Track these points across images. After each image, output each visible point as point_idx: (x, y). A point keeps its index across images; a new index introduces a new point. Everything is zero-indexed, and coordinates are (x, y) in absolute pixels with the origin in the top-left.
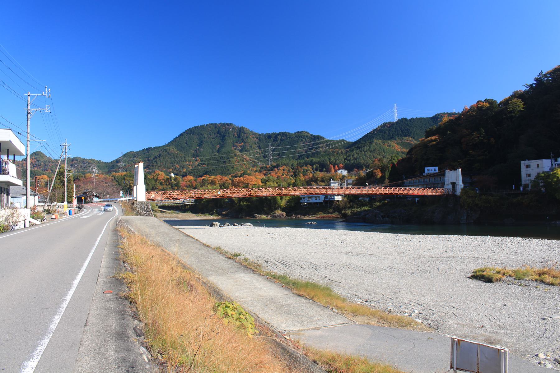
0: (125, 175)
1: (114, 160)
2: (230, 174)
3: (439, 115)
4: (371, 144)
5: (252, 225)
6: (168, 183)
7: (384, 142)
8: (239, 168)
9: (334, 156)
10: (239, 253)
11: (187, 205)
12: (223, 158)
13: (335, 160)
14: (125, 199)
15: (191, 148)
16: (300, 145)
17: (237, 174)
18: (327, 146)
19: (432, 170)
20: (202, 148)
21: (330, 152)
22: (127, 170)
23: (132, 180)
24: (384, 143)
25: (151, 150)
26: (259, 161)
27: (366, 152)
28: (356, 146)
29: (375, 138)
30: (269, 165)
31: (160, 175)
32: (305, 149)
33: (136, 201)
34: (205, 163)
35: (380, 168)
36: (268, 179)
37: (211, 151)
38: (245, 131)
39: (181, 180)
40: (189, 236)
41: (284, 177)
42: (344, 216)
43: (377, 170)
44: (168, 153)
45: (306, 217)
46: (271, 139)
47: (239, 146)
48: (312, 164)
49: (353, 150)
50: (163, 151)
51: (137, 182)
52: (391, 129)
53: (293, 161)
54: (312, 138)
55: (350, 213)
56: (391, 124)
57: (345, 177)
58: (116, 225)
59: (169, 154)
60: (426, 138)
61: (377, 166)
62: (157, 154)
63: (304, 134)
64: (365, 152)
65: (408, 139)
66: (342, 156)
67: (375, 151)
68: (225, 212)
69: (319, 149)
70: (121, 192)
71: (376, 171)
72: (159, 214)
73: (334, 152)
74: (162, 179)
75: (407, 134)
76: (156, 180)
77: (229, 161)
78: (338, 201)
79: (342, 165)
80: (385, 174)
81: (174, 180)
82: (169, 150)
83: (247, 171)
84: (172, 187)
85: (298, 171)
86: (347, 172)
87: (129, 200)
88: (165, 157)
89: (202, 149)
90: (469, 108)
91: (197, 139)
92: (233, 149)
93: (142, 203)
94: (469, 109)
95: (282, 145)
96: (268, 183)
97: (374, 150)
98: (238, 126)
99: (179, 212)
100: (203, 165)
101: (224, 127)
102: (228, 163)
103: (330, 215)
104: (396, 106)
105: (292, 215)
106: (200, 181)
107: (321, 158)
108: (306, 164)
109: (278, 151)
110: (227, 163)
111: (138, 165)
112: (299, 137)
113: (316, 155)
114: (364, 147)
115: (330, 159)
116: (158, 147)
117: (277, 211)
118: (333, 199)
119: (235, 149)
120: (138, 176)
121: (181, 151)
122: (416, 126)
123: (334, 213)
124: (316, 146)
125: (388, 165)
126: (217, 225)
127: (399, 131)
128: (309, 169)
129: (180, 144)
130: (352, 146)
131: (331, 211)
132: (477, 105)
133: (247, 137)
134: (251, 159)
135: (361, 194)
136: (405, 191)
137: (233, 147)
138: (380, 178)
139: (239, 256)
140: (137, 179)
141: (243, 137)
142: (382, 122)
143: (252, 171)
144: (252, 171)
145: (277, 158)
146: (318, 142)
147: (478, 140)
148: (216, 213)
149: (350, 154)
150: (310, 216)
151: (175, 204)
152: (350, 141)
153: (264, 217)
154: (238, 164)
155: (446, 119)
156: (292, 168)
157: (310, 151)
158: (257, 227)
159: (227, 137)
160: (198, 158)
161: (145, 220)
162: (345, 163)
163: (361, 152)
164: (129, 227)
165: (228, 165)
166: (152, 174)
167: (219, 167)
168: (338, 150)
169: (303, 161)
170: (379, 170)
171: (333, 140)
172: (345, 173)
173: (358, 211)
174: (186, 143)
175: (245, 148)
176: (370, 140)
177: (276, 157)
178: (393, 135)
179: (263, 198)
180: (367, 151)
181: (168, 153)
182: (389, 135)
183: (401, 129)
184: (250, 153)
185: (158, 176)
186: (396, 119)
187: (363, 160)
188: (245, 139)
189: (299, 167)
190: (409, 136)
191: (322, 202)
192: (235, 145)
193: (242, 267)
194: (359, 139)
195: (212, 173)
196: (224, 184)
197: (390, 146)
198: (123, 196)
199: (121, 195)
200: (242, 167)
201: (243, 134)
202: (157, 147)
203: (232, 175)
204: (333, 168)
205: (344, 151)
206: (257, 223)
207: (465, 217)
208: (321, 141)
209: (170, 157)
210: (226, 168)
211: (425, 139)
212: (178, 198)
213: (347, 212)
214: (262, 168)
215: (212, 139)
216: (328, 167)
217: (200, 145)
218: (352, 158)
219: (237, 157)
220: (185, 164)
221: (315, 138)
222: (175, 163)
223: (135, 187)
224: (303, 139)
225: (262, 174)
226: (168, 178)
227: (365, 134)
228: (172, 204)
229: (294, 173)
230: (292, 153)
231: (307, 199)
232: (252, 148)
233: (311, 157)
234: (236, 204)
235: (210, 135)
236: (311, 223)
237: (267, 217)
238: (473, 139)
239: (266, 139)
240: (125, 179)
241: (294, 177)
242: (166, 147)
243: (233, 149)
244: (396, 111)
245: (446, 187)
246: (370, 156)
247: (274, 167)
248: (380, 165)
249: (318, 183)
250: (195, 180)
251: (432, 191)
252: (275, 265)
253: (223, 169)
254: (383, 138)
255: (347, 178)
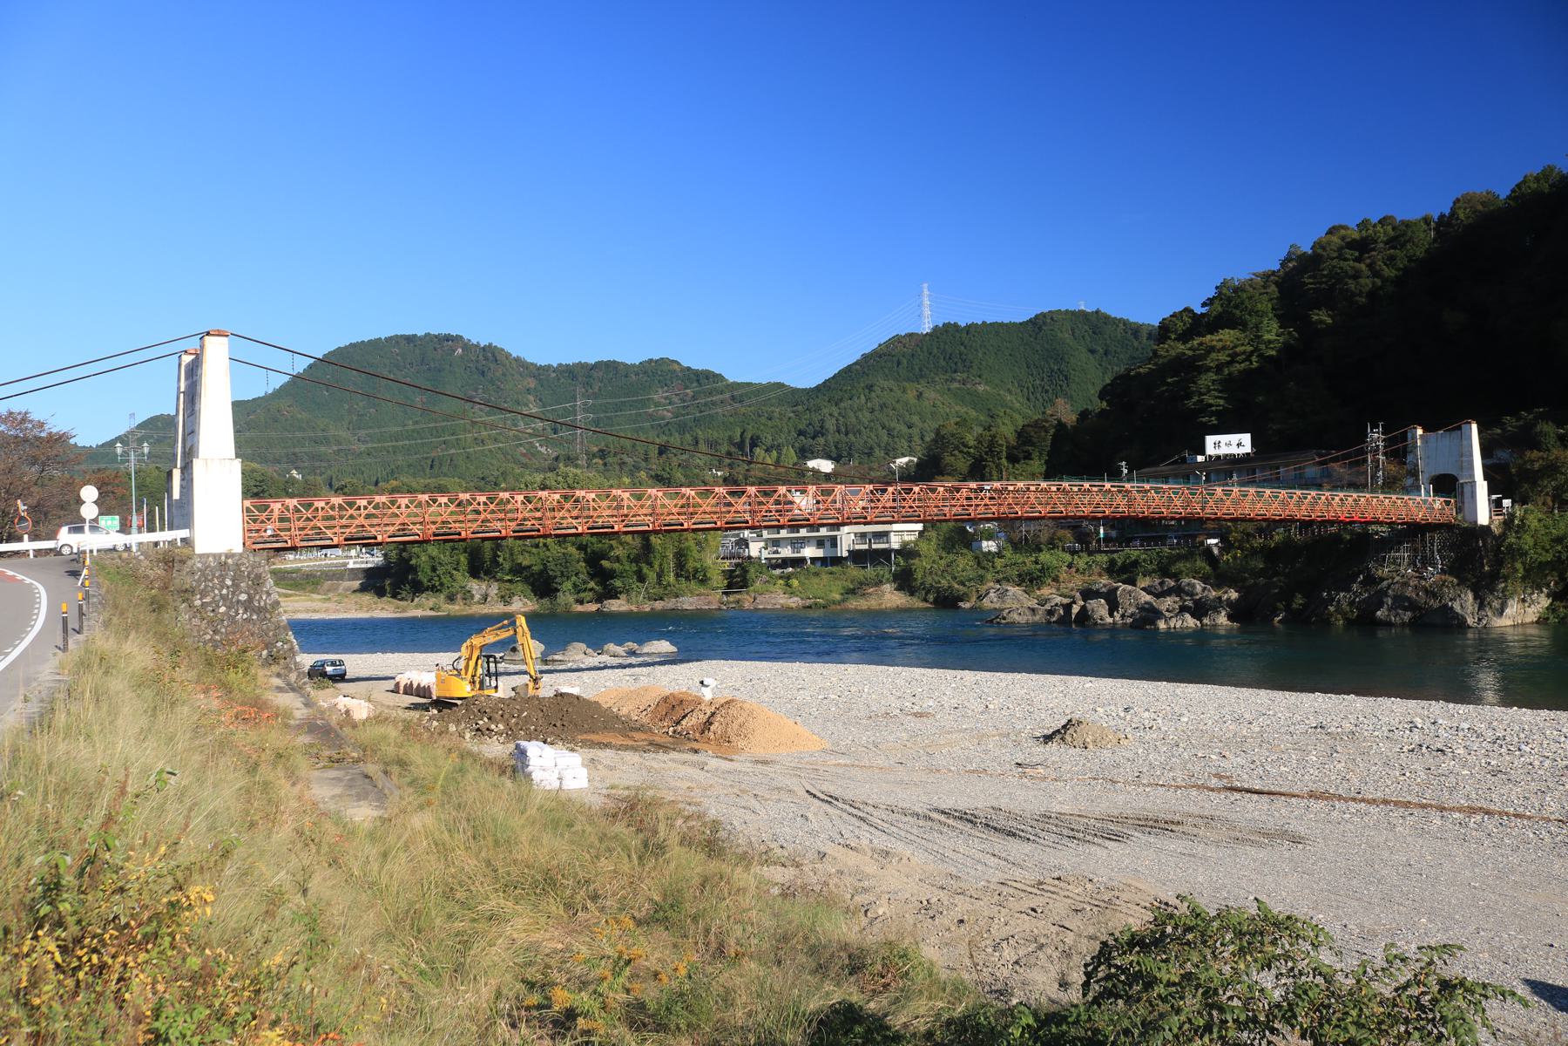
3: (1043, 315)
93: (222, 564)
171: (749, 384)
178: (921, 370)
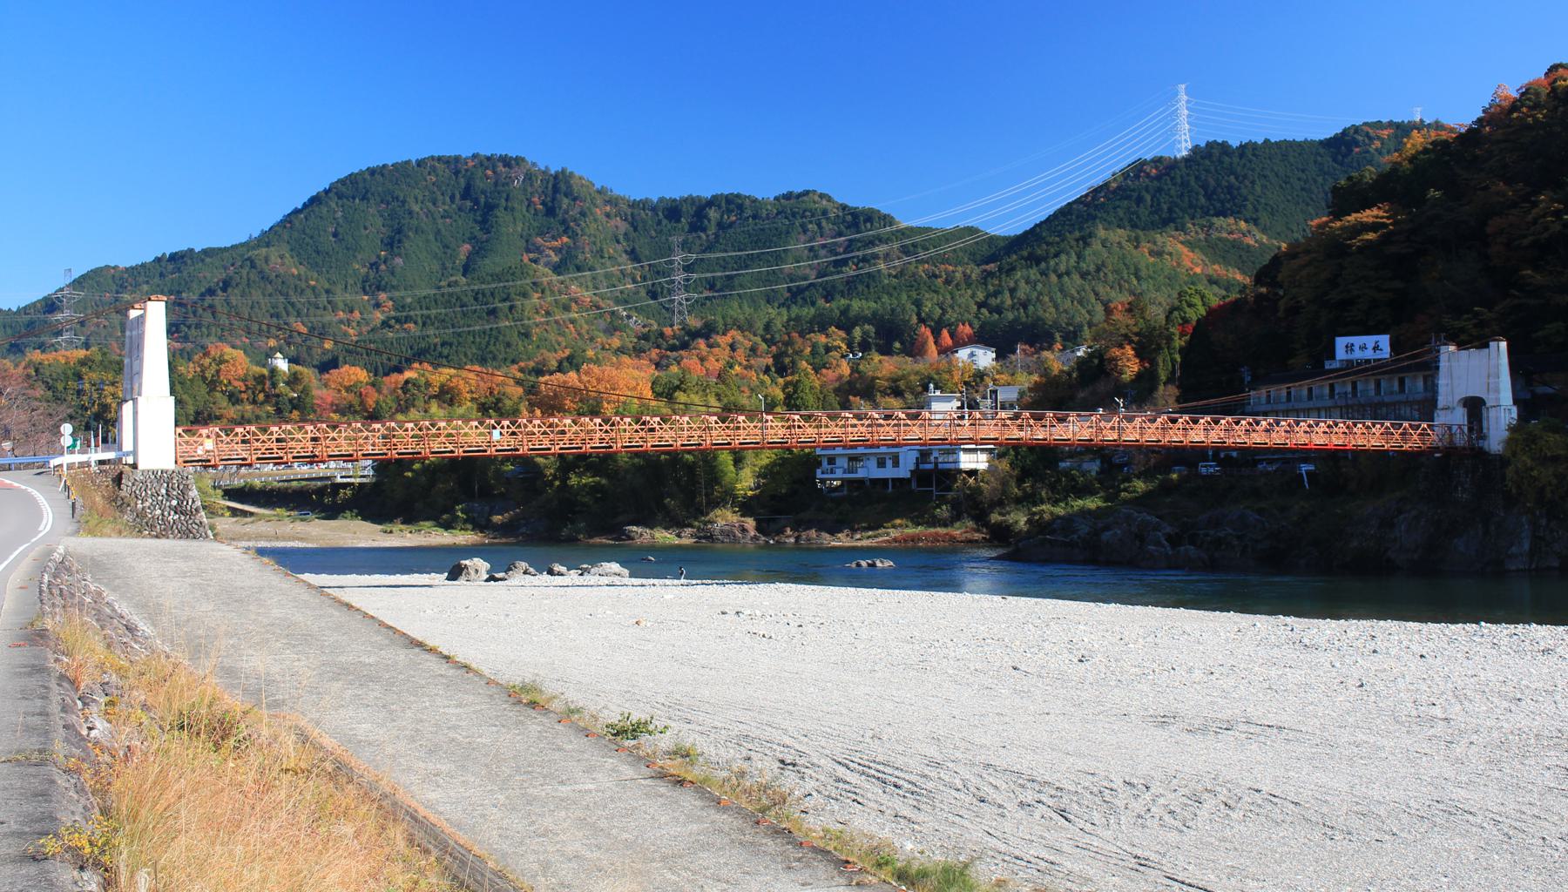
0: (83, 363)
1: (34, 300)
2: (513, 362)
3: (1356, 129)
4: (1087, 244)
5: (626, 572)
6: (261, 397)
7: (1137, 239)
8: (552, 337)
9: (935, 292)
10: (644, 717)
11: (345, 486)
12: (484, 295)
13: (942, 308)
14: (83, 458)
15: (355, 257)
16: (798, 245)
17: (544, 362)
18: (905, 251)
19: (1364, 348)
20: (399, 255)
21: (921, 276)
22: (92, 340)
23: (113, 384)
24: (1138, 243)
25: (189, 262)
26: (630, 308)
27: (1066, 278)
28: (1025, 253)
29: (1098, 221)
30: (672, 326)
31: (227, 361)
32: (816, 262)
33: (134, 466)
34: (411, 317)
35: (1136, 339)
36: (682, 383)
37: (436, 266)
38: (576, 189)
39: (315, 382)
40: (420, 645)
41: (737, 375)
42: (1000, 535)
43: (1121, 346)
44: (261, 272)
45: (842, 540)
46: (678, 221)
47: (551, 248)
48: (846, 323)
49: (1012, 269)
50: (241, 267)
51: (136, 387)
52: (1166, 184)
53: (770, 310)
54: (844, 221)
55: (1026, 523)
56: (1166, 168)
57: (988, 376)
58: (41, 592)
59: (264, 278)
60: (1337, 214)
61: (1123, 331)
62: (214, 276)
63: (814, 202)
64: (1060, 276)
65: (1234, 227)
66: (969, 292)
67: (1102, 274)
68: (502, 515)
69: (875, 265)
70: (67, 428)
71: (1116, 352)
72: (225, 524)
73: (936, 276)
74: (238, 380)
75: (1228, 206)
76: (212, 385)
77: (511, 308)
78: (973, 473)
79: (967, 330)
80: (1153, 362)
81: (287, 383)
82: (267, 260)
83: (584, 351)
84: (279, 411)
85: (790, 351)
86: (994, 355)
87: (101, 462)
88: (247, 290)
89: (399, 261)
90: (1517, 95)
91: (379, 221)
92: (526, 261)
93: (160, 476)
94: (1516, 100)
95: (723, 247)
96: (681, 397)
97: (1098, 270)
98: (546, 167)
99: (311, 516)
100: (406, 326)
101: (489, 172)
102: (507, 318)
103: (941, 530)
104: (1186, 94)
105: (781, 531)
106: (393, 386)
107: (885, 299)
108: (822, 324)
109: (708, 271)
110: (501, 314)
111: (142, 312)
112: (794, 215)
113: (860, 288)
114: (1057, 255)
115: (918, 304)
116: (220, 249)
117: (718, 512)
118: (952, 466)
119: (535, 261)
120: (140, 358)
121: (314, 266)
122: (1265, 177)
123: (958, 524)
124: (860, 253)
125: (1167, 329)
126: (477, 571)
127: (1197, 194)
128: (835, 344)
129: (312, 237)
130: (1008, 254)
131: (946, 515)
132: (1551, 80)
133: (583, 214)
134: (601, 304)
135: (1096, 445)
136: (1274, 435)
137: (528, 251)
138: (1132, 381)
139: (647, 736)
140: (135, 369)
141: (566, 212)
142: (1128, 156)
143: (603, 348)
144: (603, 348)
145: (706, 298)
146: (868, 236)
147: (1557, 227)
148: (465, 521)
149: (1000, 285)
150: (858, 536)
151: (294, 484)
152: (997, 233)
153: (664, 536)
154: (547, 323)
155: (1417, 141)
156: (765, 340)
157: (838, 273)
158: (652, 581)
159: (500, 213)
160: (383, 296)
161: (186, 558)
162: (979, 318)
163: (1046, 275)
164: (109, 596)
165: (507, 323)
166: (196, 357)
167: (469, 332)
168: (951, 268)
169: (808, 312)
170: (1128, 347)
172: (985, 358)
173: (1059, 517)
174: (335, 235)
175: (577, 257)
176: (1081, 229)
177: (701, 293)
178: (1170, 210)
179: (663, 457)
180: (1068, 273)
181: (261, 272)
182: (1156, 209)
183: (1205, 187)
184: (594, 278)
185: (222, 366)
186: (1184, 145)
187: (1053, 310)
188: (575, 220)
189: (795, 335)
190: (1236, 212)
191: (908, 475)
192: (533, 244)
193: (770, 843)
194: (1036, 225)
195: (441, 355)
196: (499, 400)
197: (1158, 254)
198: (74, 445)
199: (67, 441)
200: (562, 334)
201: (566, 201)
202: (214, 249)
203: (522, 364)
204: (931, 340)
205: (975, 272)
206: (648, 564)
207: (1526, 546)
208: (882, 230)
209: (270, 289)
210: (497, 338)
211: (1331, 221)
212: (315, 456)
213: (1011, 518)
214: (645, 337)
215: (440, 221)
216: (911, 337)
217: (393, 242)
218: (1009, 302)
219: (543, 292)
220: (329, 317)
221: (857, 219)
222: (288, 315)
223: (127, 408)
224: (811, 222)
225: (645, 362)
226: (263, 376)
227: (1058, 207)
228: (279, 481)
229: (777, 358)
230: (768, 279)
231: (846, 466)
232: (602, 257)
233: (843, 296)
234: (551, 484)
235: (434, 204)
236: (869, 565)
237: (679, 536)
238: (1535, 222)
239: (659, 223)
240: (79, 377)
241: (776, 375)
242: (253, 248)
243: (526, 261)
244: (1186, 112)
245: (1441, 418)
246: (1083, 294)
247: (695, 334)
248: (1136, 329)
249: (878, 397)
250: (373, 385)
251: (1387, 433)
252: (841, 785)
253: (484, 342)
254: (1130, 220)
255: (994, 380)
